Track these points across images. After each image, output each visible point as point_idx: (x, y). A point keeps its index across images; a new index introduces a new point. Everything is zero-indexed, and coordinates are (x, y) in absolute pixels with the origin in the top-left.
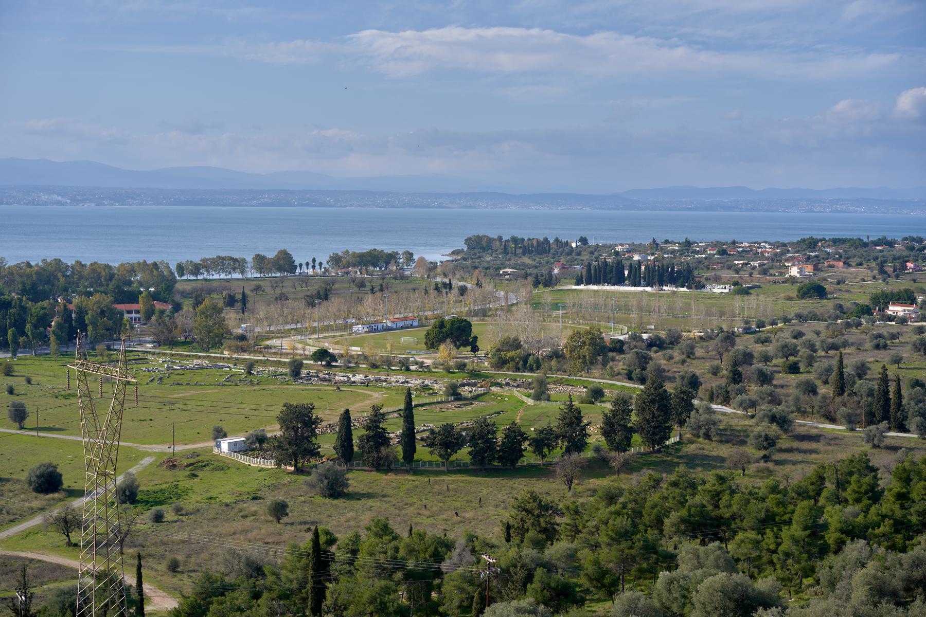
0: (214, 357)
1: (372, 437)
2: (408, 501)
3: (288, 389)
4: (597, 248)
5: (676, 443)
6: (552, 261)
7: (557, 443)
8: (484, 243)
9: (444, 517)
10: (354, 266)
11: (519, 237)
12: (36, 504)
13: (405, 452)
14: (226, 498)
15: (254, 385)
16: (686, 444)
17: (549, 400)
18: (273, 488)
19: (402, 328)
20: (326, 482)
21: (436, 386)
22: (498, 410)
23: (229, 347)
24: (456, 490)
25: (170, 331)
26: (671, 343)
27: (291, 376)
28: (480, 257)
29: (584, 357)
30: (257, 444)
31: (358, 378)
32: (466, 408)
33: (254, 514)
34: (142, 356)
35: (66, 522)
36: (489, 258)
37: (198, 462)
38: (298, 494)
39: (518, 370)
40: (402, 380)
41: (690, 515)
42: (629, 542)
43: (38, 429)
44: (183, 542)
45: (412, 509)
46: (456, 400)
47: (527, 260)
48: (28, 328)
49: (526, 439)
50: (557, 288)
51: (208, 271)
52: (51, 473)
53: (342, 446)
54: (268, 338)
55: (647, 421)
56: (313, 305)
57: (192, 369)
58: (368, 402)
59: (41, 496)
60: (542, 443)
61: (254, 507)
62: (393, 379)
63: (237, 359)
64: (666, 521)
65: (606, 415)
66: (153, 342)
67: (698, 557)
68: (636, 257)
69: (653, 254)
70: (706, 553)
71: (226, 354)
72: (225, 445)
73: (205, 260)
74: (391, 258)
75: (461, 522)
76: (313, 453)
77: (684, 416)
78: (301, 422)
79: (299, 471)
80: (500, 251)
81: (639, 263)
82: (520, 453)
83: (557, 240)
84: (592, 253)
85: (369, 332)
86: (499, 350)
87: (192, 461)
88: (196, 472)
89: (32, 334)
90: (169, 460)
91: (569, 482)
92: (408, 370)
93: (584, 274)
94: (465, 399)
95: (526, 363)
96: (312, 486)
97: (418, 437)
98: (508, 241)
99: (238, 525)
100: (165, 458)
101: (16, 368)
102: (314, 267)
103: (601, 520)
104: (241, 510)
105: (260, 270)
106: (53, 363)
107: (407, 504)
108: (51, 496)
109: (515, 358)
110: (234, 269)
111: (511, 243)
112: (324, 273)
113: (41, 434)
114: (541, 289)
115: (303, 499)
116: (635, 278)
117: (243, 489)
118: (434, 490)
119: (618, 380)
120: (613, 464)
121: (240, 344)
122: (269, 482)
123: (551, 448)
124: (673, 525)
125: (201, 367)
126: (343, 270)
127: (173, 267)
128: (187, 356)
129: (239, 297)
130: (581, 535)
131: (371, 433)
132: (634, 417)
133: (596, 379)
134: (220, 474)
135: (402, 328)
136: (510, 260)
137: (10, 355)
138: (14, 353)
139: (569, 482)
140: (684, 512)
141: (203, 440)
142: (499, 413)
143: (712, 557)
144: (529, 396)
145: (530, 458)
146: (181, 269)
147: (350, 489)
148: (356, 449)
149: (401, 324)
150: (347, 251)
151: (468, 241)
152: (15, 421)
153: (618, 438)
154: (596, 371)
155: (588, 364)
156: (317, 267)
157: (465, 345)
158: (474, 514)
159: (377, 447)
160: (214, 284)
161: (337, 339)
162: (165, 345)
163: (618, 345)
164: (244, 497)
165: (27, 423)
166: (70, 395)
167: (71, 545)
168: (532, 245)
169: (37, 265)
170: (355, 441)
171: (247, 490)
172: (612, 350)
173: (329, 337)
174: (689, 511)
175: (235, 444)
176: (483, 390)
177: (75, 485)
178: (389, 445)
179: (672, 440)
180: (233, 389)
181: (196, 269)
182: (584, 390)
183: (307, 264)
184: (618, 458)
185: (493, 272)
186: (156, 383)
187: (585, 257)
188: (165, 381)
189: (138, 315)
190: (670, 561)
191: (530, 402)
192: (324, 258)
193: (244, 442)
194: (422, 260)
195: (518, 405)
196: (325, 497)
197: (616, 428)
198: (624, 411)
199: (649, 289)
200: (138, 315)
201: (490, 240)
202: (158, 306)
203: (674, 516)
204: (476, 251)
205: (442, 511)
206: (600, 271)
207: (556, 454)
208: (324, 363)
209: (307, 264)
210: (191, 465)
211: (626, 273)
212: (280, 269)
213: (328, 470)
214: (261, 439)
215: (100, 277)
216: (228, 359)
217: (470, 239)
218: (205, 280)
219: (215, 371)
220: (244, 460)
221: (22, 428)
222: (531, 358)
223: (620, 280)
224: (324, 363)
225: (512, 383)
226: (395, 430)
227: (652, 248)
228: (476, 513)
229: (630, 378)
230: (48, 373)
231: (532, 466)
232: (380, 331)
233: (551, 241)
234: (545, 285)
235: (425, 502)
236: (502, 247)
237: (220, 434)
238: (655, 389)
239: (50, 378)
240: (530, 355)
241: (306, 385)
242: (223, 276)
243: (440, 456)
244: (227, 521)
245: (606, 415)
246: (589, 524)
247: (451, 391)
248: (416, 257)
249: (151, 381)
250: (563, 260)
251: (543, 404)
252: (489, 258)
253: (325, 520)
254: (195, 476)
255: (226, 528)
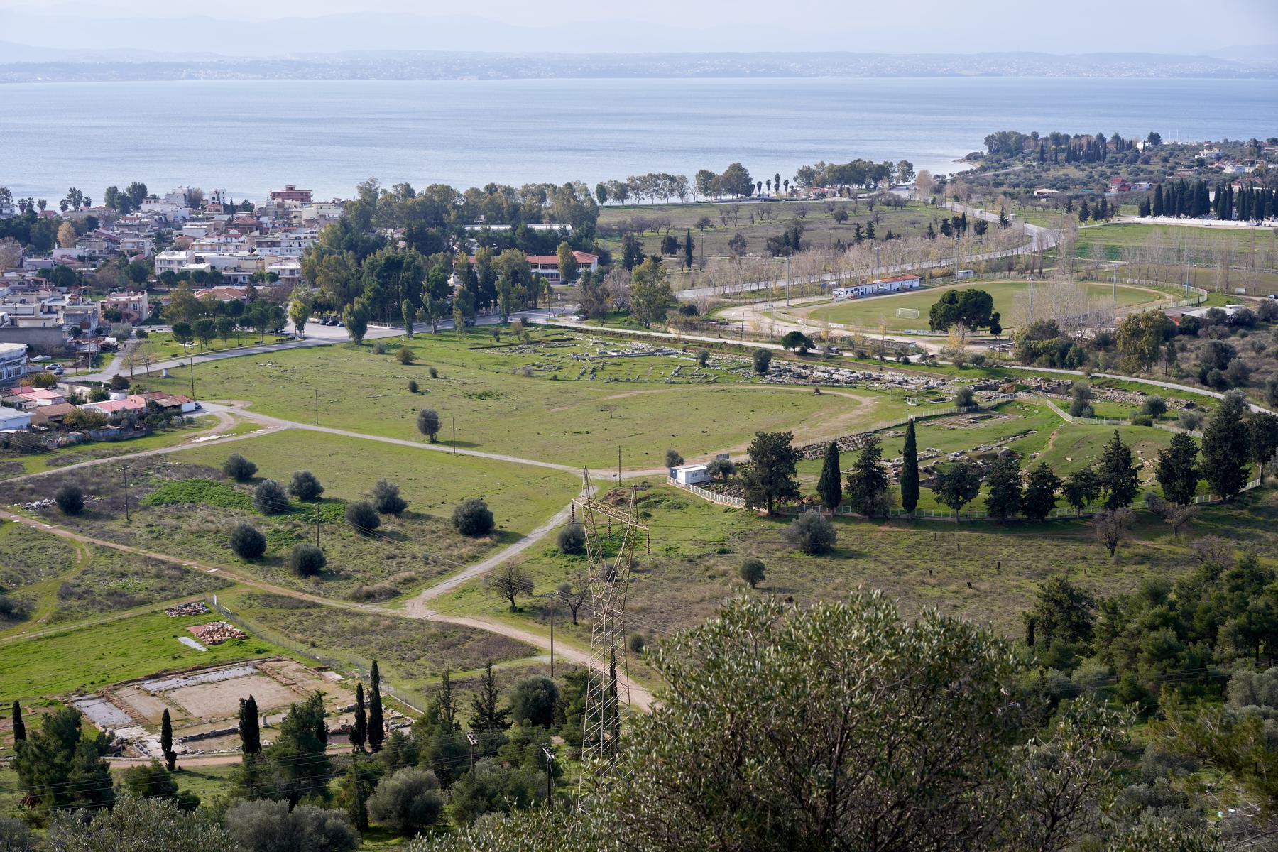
0: (657, 338)
1: (866, 478)
2: (909, 562)
3: (754, 390)
4: (1176, 150)
5: (1256, 489)
6: (1109, 172)
7: (1099, 491)
8: (1012, 142)
9: (953, 588)
10: (833, 184)
11: (1063, 133)
12: (466, 550)
13: (906, 497)
14: (688, 550)
15: (709, 382)
16: (1268, 490)
17: (1092, 416)
18: (744, 536)
19: (898, 291)
20: (808, 535)
21: (945, 389)
22: (1025, 428)
23: (676, 323)
24: (968, 549)
25: (601, 300)
26: (1266, 320)
27: (757, 370)
28: (1005, 166)
29: (1142, 351)
30: (720, 475)
31: (843, 374)
32: (983, 424)
33: (724, 574)
34: (567, 335)
35: (509, 583)
36: (1019, 167)
37: (650, 496)
38: (774, 547)
39: (1053, 365)
40: (899, 379)
41: (1251, 622)
42: (1172, 661)
43: (454, 444)
44: (643, 610)
45: (913, 574)
46: (970, 411)
47: (1072, 171)
48: (426, 297)
49: (1059, 485)
50: (1115, 220)
51: (637, 194)
52: (481, 511)
53: (828, 488)
54: (722, 306)
55: (1217, 462)
56: (777, 253)
57: (631, 356)
58: (856, 412)
59: (470, 540)
60: (1081, 489)
61: (722, 564)
62: (888, 376)
63: (687, 342)
64: (1221, 628)
65: (1163, 456)
66: (577, 313)
67: (1251, 684)
68: (1229, 169)
69: (1253, 163)
70: (1259, 679)
71: (673, 333)
72: (682, 474)
73: (633, 180)
74: (882, 172)
75: (975, 595)
76: (792, 492)
77: (1268, 450)
78: (776, 458)
79: (774, 515)
80: (1034, 155)
81: (1234, 178)
82: (1050, 503)
83: (1116, 137)
84: (1165, 160)
85: (855, 297)
86: (1028, 338)
87: (642, 494)
88: (650, 511)
89: (431, 305)
90: (616, 494)
91: (1112, 545)
92: (907, 362)
93: (1152, 197)
94: (982, 410)
95: (1064, 355)
96: (792, 539)
97: (921, 467)
98: (1046, 139)
99: (705, 589)
100: (610, 490)
101: (415, 352)
102: (777, 187)
103: (1143, 623)
104: (707, 569)
105: (706, 191)
106: (458, 346)
107: (908, 567)
108: (480, 541)
109: (1050, 348)
110: (671, 191)
111: (1050, 143)
112: (791, 195)
113: (458, 451)
114: (1091, 223)
115: (778, 554)
116: (1224, 207)
117: (707, 537)
118: (941, 549)
119: (1188, 384)
120: (1170, 521)
121: (690, 319)
122: (739, 527)
123: (1092, 497)
124: (1229, 634)
125: (643, 354)
126: (817, 191)
127: (592, 188)
128: (623, 335)
129: (682, 240)
130: (1119, 639)
131: (864, 474)
132: (1200, 457)
133: (1159, 383)
134: (676, 514)
135: (898, 291)
136: (1048, 170)
137: (405, 332)
138: (410, 330)
139: (1112, 545)
140: (1242, 619)
141: (653, 465)
142: (1026, 433)
143: (1266, 688)
144: (1065, 408)
145: (1063, 509)
146: (602, 192)
147: (838, 545)
148: (844, 492)
149: (896, 285)
150: (823, 164)
151: (989, 140)
152: (426, 432)
153: (1179, 485)
154: (1159, 369)
155: (1147, 359)
156: (782, 187)
157: (983, 324)
158: (992, 593)
159: (871, 492)
160: (649, 216)
161: (814, 308)
162: (593, 318)
163: (1192, 325)
164: (709, 549)
165: (440, 435)
166: (486, 395)
167: (514, 609)
168: (1081, 146)
169: (420, 194)
170: (844, 483)
171: (712, 538)
172: (1184, 331)
173: (802, 305)
174: (1249, 618)
175: (694, 474)
176: (1003, 398)
177: (507, 524)
178: (884, 489)
179: (1251, 484)
180: (683, 388)
181: (622, 192)
182: (1141, 397)
183: (768, 183)
184: (1177, 512)
185: (1023, 193)
186: (588, 377)
187: (1155, 166)
188: (599, 374)
189: (556, 271)
190: (1218, 687)
191: (1068, 418)
192: (789, 172)
193: (705, 472)
194: (924, 173)
195: (1053, 431)
196: (807, 553)
197: (1176, 471)
198: (1186, 452)
199: (1243, 224)
200: (556, 271)
201: (1021, 139)
202: (580, 257)
203: (1231, 623)
204: (1000, 155)
205: (951, 578)
206: (1175, 197)
207: (1096, 507)
208: (797, 349)
209: (768, 183)
210: (642, 499)
211: (1212, 197)
212: (732, 191)
213: (811, 521)
214: (726, 469)
215: (497, 203)
216: (675, 341)
217: (993, 137)
218: (634, 207)
219: (658, 359)
220: (706, 495)
221: (433, 442)
222: (1072, 349)
223: (1201, 210)
224: (797, 349)
225: (1045, 386)
226: (891, 461)
227: (1251, 154)
228: (993, 585)
229: (1203, 381)
230: (455, 361)
231: (1066, 520)
232: (869, 295)
233: (1109, 139)
234: (1096, 217)
235: (930, 564)
236: (1038, 149)
237: (674, 460)
238: (1229, 422)
239: (458, 369)
240: (1070, 345)
241: (776, 384)
242: (657, 201)
243: (950, 504)
244: (691, 582)
245: (1163, 456)
246: (1129, 626)
247: (964, 400)
248: (917, 170)
249: (582, 374)
250: (1124, 174)
251: (1084, 420)
252: (1019, 167)
253: (809, 585)
254: (648, 515)
255: (691, 593)
